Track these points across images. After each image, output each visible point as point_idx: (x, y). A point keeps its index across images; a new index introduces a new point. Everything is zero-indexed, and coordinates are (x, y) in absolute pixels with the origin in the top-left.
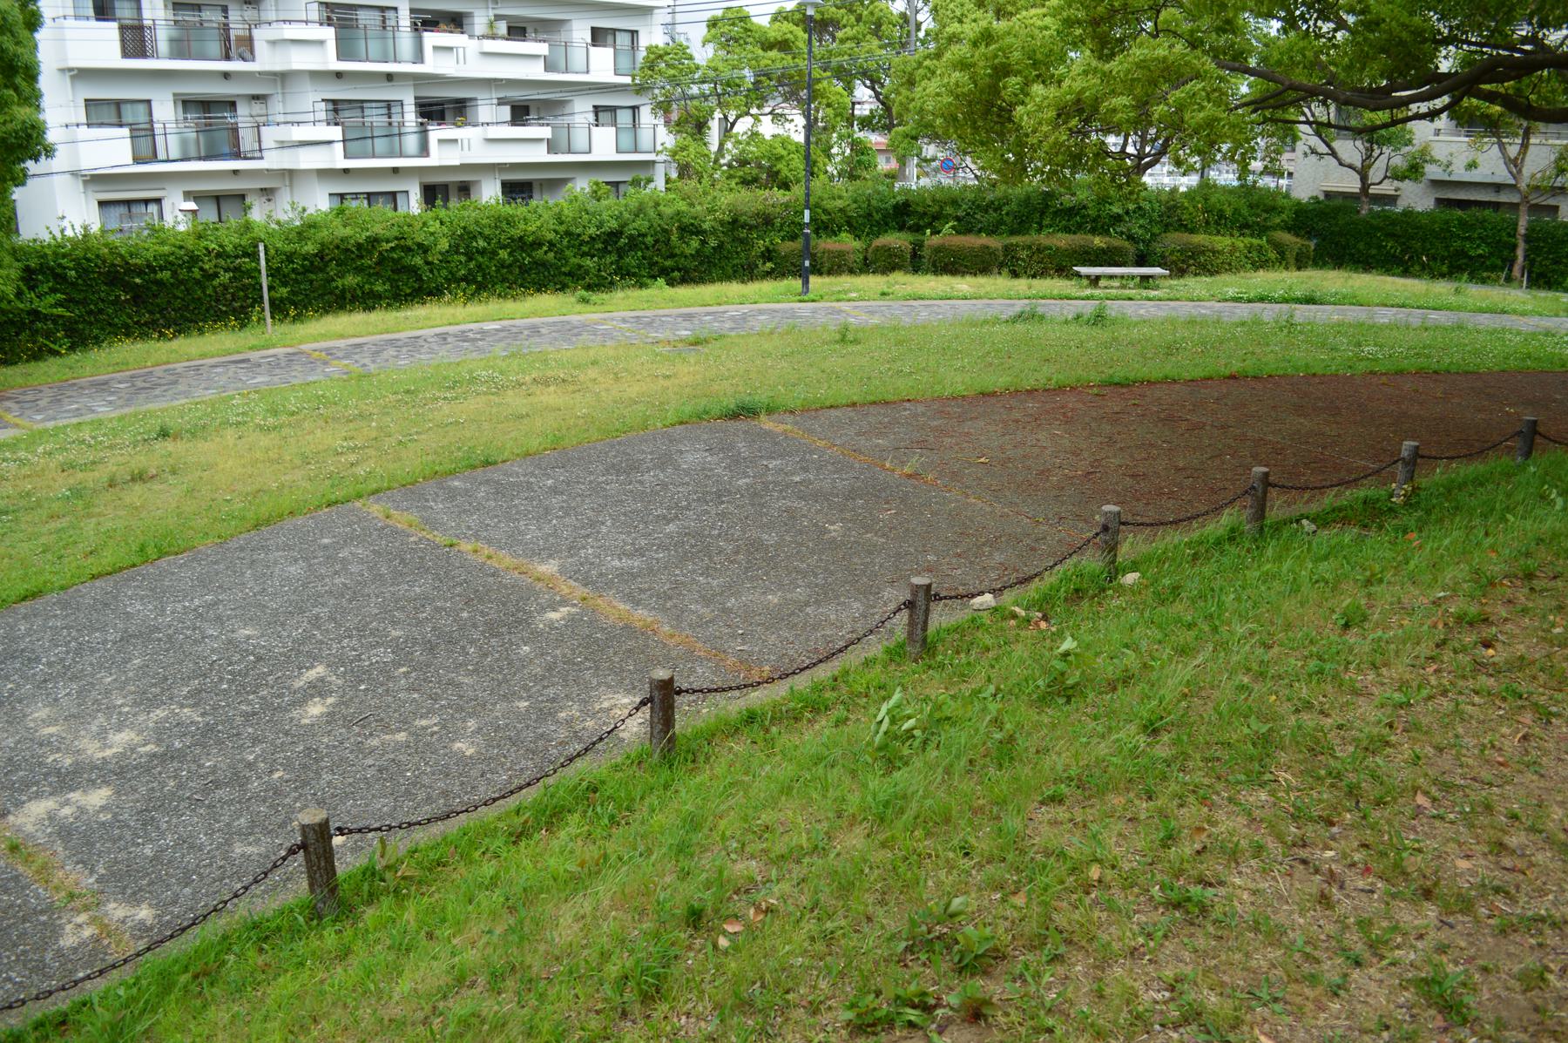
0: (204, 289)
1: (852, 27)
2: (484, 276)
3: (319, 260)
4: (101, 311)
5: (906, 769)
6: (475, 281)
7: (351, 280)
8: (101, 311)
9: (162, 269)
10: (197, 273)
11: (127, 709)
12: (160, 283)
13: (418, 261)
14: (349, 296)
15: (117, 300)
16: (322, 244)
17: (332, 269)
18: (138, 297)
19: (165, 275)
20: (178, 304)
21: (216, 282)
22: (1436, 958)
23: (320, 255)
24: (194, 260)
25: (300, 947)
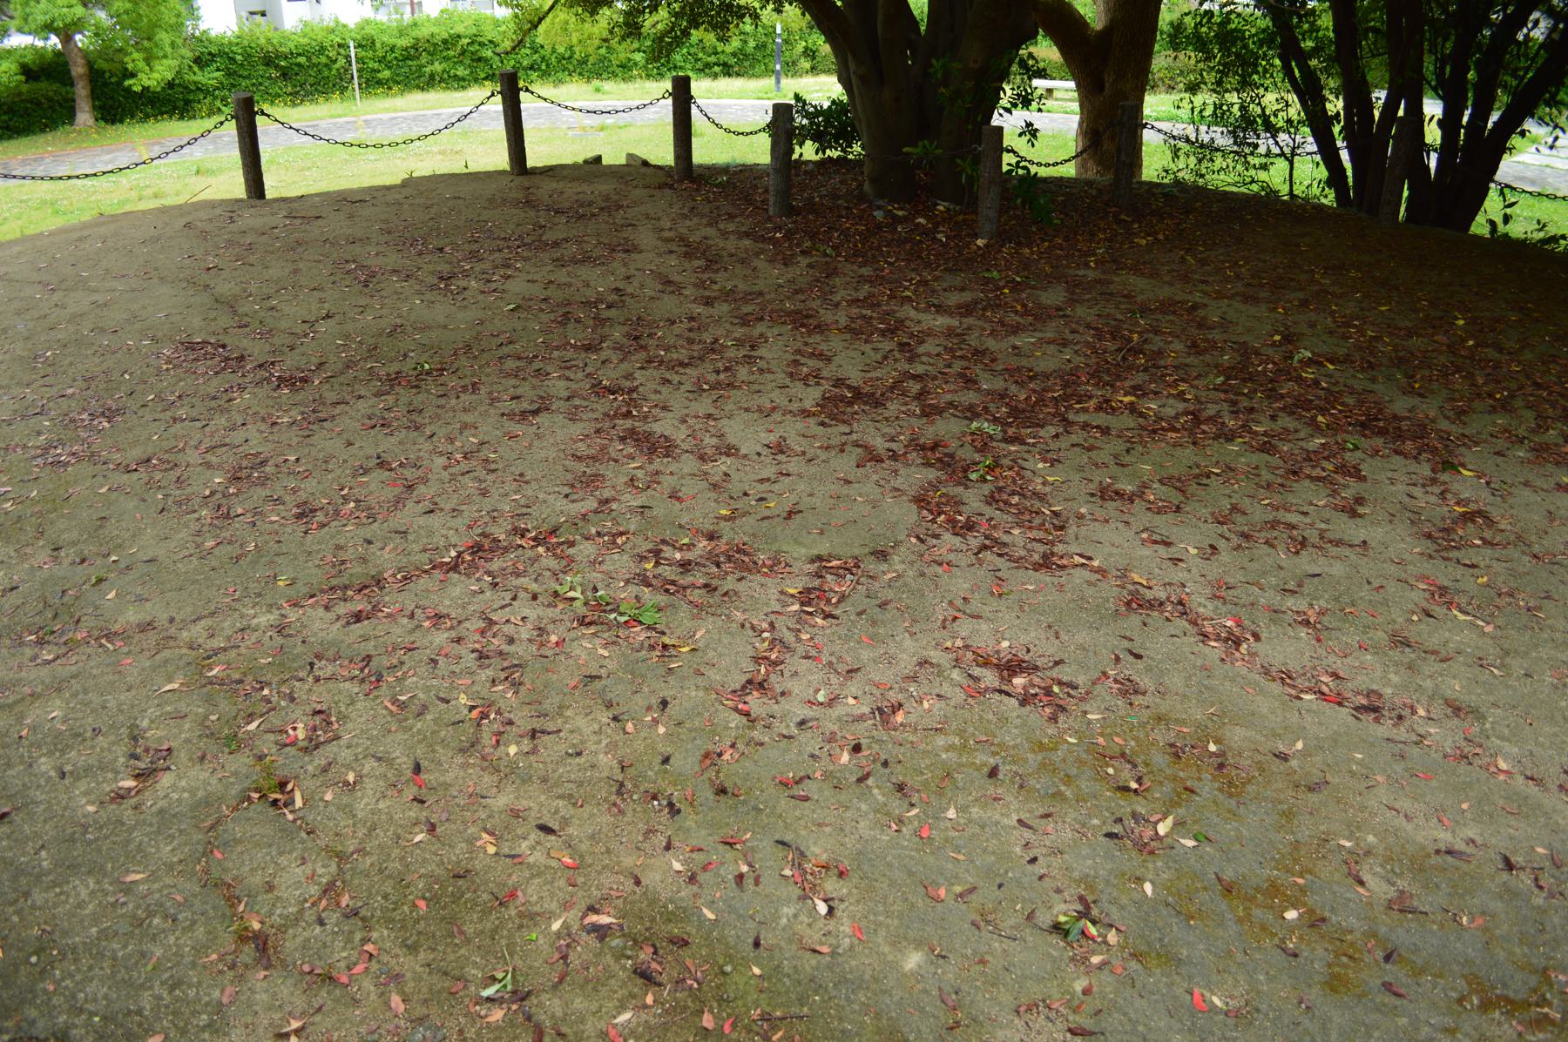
0: (330, 70)
1: (102, 750)
2: (547, 65)
3: (412, 53)
4: (261, 84)
5: (463, 578)
6: (539, 69)
7: (438, 67)
8: (261, 84)
9: (299, 55)
10: (323, 60)
11: (1196, 277)
12: (299, 65)
13: (489, 53)
14: (438, 78)
15: (270, 78)
16: (417, 39)
17: (424, 58)
18: (285, 75)
19: (302, 60)
20: (311, 80)
21: (336, 66)
22: (1052, 894)
23: (415, 47)
24: (322, 49)
25: (97, 159)
